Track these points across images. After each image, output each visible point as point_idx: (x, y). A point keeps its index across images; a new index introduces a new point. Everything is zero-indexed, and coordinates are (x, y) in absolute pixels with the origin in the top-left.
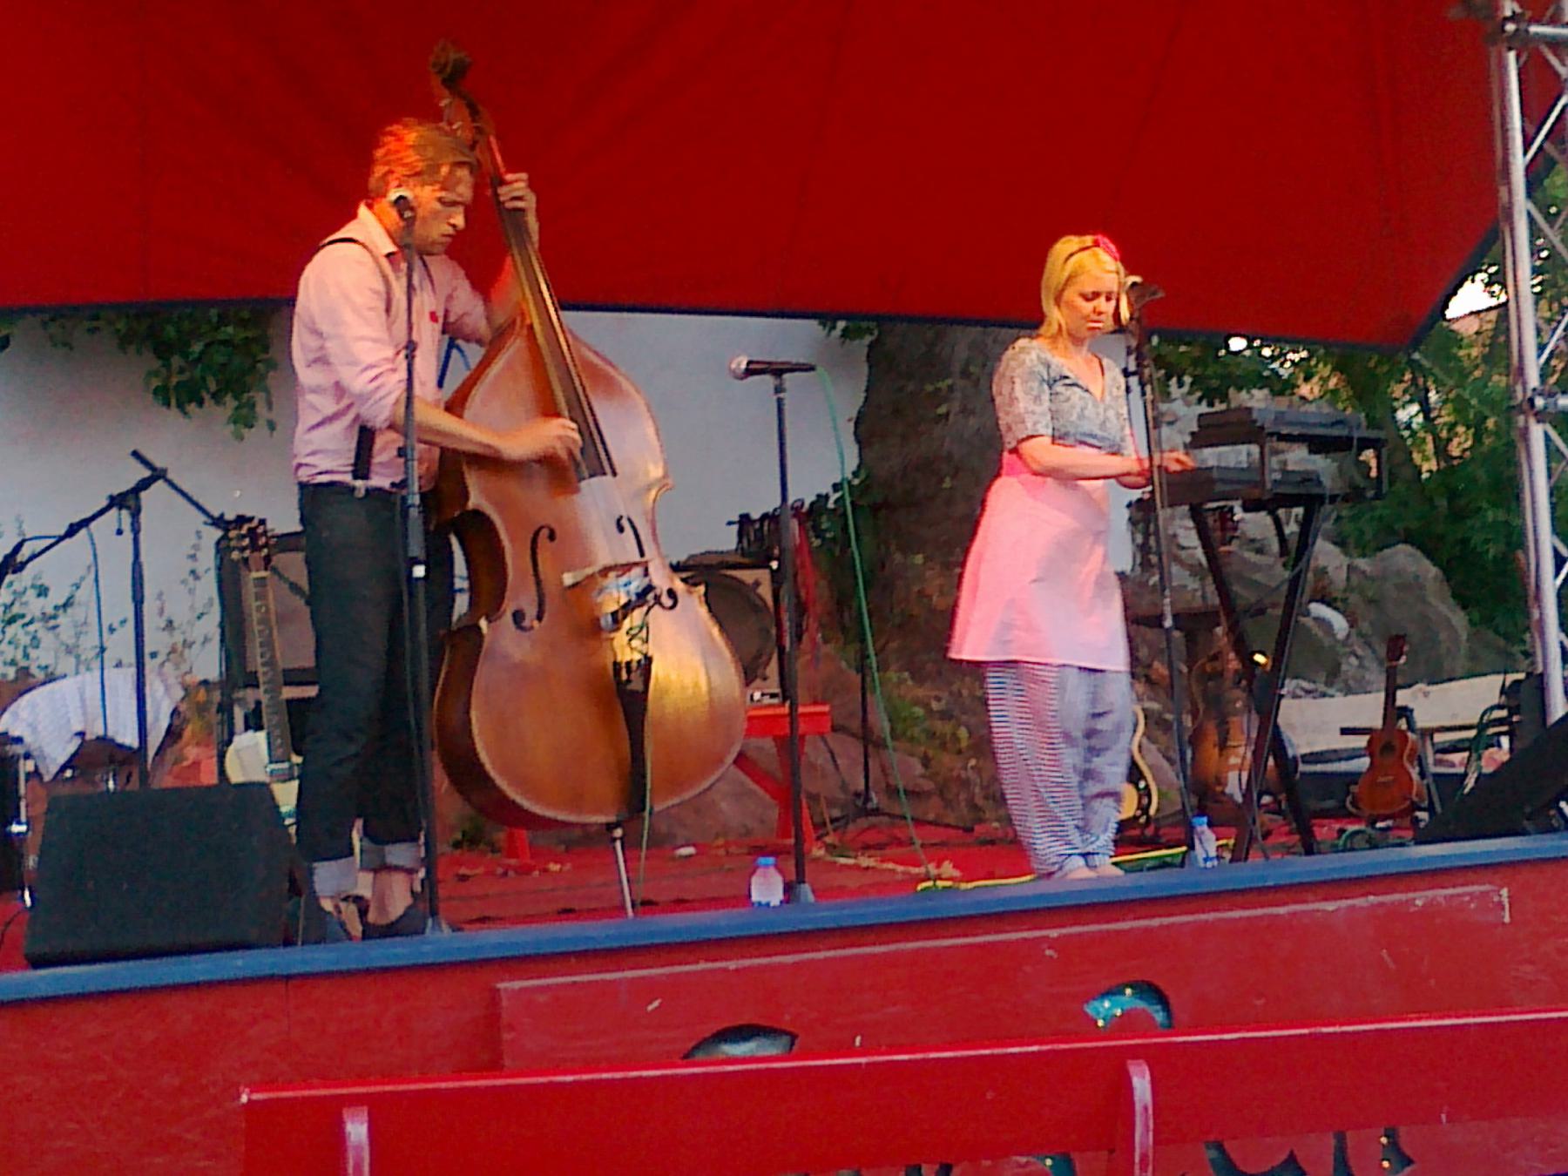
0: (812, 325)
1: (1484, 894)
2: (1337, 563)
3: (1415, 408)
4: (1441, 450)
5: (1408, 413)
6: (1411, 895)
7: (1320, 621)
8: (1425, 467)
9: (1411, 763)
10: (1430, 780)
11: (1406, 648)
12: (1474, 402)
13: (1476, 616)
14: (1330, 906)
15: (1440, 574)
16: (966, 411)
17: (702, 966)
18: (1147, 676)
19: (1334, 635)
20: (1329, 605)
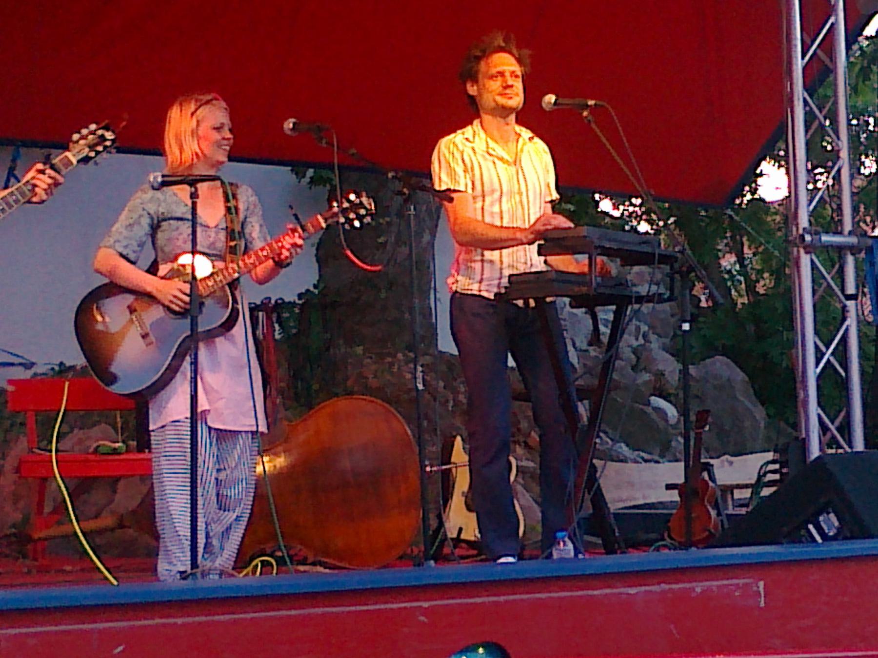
0: (283, 172)
1: (746, 585)
2: (671, 369)
3: (733, 258)
4: (751, 288)
5: (728, 261)
6: (694, 584)
7: (657, 410)
8: (740, 301)
9: (710, 503)
10: (724, 518)
11: (710, 419)
12: (776, 253)
13: (772, 412)
14: (632, 591)
15: (747, 379)
16: (398, 243)
17: (158, 621)
18: (525, 442)
19: (667, 421)
20: (665, 398)
